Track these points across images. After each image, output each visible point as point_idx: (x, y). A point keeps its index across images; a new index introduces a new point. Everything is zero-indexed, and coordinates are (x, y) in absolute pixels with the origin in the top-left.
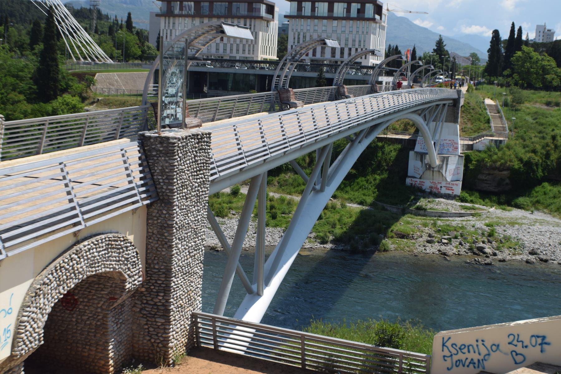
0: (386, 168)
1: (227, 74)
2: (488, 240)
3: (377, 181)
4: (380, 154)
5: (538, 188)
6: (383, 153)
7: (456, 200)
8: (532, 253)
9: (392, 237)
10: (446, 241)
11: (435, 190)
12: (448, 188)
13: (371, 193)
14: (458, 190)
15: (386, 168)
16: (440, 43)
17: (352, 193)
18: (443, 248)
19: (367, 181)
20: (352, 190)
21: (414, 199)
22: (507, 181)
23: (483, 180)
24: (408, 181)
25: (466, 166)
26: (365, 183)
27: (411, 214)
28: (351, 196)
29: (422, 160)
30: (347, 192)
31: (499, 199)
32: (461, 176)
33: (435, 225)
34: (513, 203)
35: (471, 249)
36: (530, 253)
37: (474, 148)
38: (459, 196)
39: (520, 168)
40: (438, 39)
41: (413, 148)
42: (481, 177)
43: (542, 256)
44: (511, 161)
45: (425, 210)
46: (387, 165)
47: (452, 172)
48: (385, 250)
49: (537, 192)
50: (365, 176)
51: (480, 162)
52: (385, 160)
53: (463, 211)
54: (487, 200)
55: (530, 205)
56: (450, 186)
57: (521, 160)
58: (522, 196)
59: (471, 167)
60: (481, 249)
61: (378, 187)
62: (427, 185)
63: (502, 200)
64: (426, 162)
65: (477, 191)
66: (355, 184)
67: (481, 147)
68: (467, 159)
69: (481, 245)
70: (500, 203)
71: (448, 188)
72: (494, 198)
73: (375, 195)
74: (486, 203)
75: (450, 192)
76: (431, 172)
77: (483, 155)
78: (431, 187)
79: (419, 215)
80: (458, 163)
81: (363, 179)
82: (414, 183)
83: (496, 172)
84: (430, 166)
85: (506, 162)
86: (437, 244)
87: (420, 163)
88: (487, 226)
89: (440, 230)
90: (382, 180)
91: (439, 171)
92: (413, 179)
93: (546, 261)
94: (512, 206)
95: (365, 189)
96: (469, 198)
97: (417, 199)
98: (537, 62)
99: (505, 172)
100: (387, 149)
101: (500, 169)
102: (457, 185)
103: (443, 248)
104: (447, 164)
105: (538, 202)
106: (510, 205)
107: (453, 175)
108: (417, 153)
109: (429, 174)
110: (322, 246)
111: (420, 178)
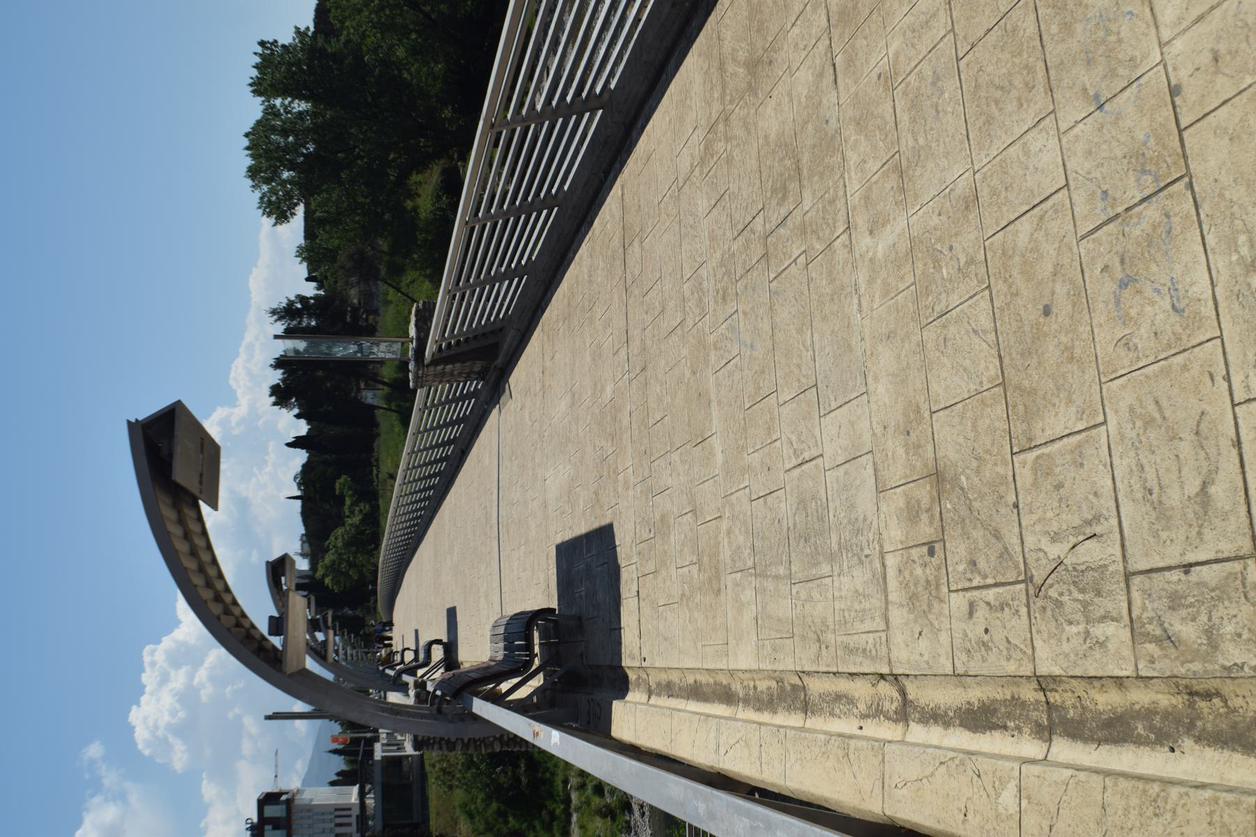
98: (340, 554)
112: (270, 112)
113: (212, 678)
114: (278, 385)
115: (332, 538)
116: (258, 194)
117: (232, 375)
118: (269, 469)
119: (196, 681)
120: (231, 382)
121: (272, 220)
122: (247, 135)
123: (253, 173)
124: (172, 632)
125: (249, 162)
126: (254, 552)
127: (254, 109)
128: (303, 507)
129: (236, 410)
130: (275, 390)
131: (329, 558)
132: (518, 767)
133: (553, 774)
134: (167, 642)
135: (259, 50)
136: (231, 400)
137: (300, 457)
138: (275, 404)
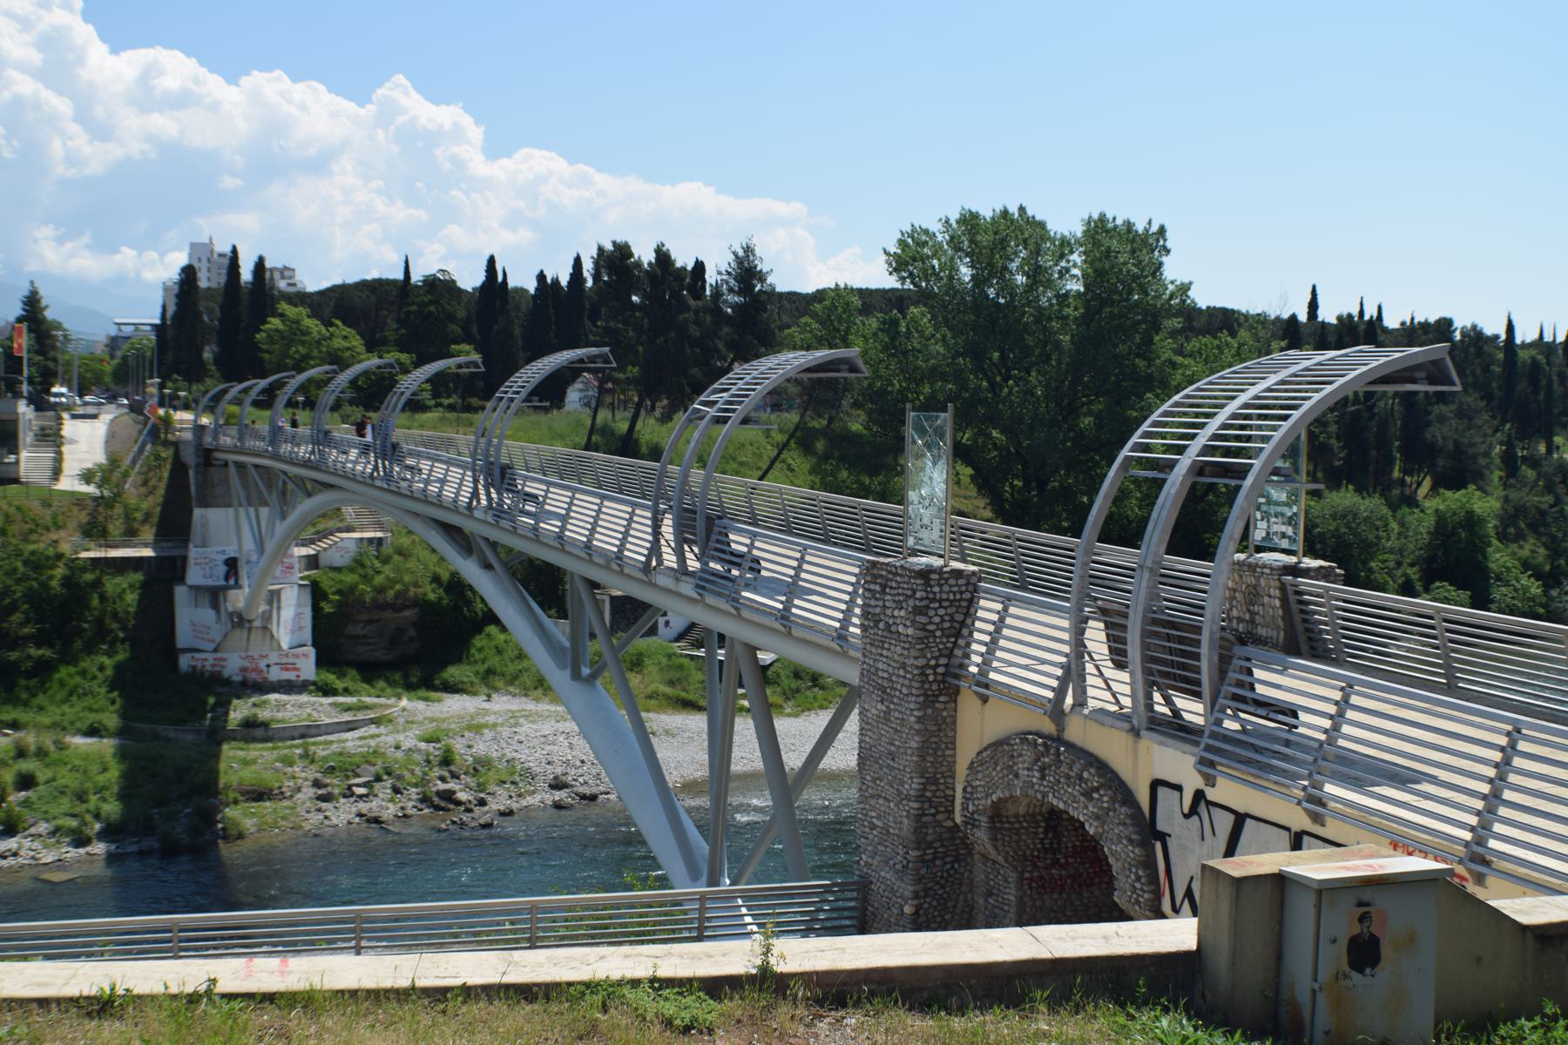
0: (121, 635)
1: (1163, 401)
2: (451, 772)
3: (109, 672)
4: (95, 602)
5: (478, 641)
6: (103, 598)
7: (310, 693)
8: (557, 785)
9: (236, 802)
10: (362, 791)
11: (253, 676)
12: (285, 667)
13: (103, 702)
14: (307, 668)
15: (121, 635)
16: (32, 304)
17: (53, 708)
18: (363, 807)
19: (83, 673)
20: (52, 701)
21: (217, 704)
22: (412, 632)
23: (357, 637)
24: (185, 662)
25: (316, 609)
26: (78, 679)
27: (235, 739)
28: (57, 718)
29: (215, 605)
30: (41, 708)
31: (406, 677)
32: (307, 635)
33: (307, 756)
34: (437, 682)
35: (425, 799)
36: (552, 787)
37: (322, 562)
38: (314, 683)
39: (440, 599)
40: (26, 293)
41: (181, 579)
42: (355, 630)
43: (581, 790)
44: (416, 585)
45: (265, 725)
46: (124, 628)
47: (291, 620)
48: (241, 836)
49: (480, 650)
50: (73, 661)
51: (346, 592)
52: (115, 616)
53: (347, 717)
54: (381, 684)
55: (476, 681)
56: (290, 660)
57: (436, 579)
58: (453, 663)
59: (328, 608)
60: (448, 796)
61: (115, 684)
62: (233, 665)
63: (414, 680)
64: (230, 609)
65: (350, 664)
66: (56, 686)
67: (336, 558)
68: (317, 593)
69: (441, 786)
70: (410, 687)
71: (285, 667)
72: (397, 677)
73: (117, 706)
74: (382, 690)
75: (291, 676)
76: (245, 633)
77: (350, 578)
78: (244, 670)
79: (254, 740)
80: (299, 605)
81: (72, 669)
82: (199, 664)
83: (388, 614)
84: (240, 617)
85: (407, 590)
86: (342, 800)
87: (211, 613)
88: (428, 741)
89: (333, 768)
90: (119, 667)
91: (265, 628)
92: (197, 655)
93: (593, 798)
94: (436, 689)
95: (85, 694)
96: (339, 685)
97: (224, 705)
98: (318, 343)
99: (408, 613)
100: (112, 584)
101: (395, 607)
102: (305, 655)
103: (363, 807)
104: (279, 608)
105: (490, 672)
106: (431, 687)
107: (293, 632)
108: (196, 589)
109: (239, 636)
110: (82, 851)
111: (215, 650)
112: (1064, 246)
113: (18, 102)
114: (631, 255)
115: (347, 331)
116: (935, 227)
117: (537, 152)
118: (380, 205)
119: (15, 75)
120: (553, 154)
121: (893, 249)
122: (1022, 209)
123: (970, 221)
124: (103, 39)
125: (986, 213)
126: (239, 182)
127: (1065, 222)
128: (393, 283)
129: (480, 158)
130: (623, 251)
131: (314, 326)
132: (39, 646)
133: (26, 704)
134: (85, 33)
135: (1154, 228)
136: (493, 150)
137: (470, 279)
138: (601, 249)
